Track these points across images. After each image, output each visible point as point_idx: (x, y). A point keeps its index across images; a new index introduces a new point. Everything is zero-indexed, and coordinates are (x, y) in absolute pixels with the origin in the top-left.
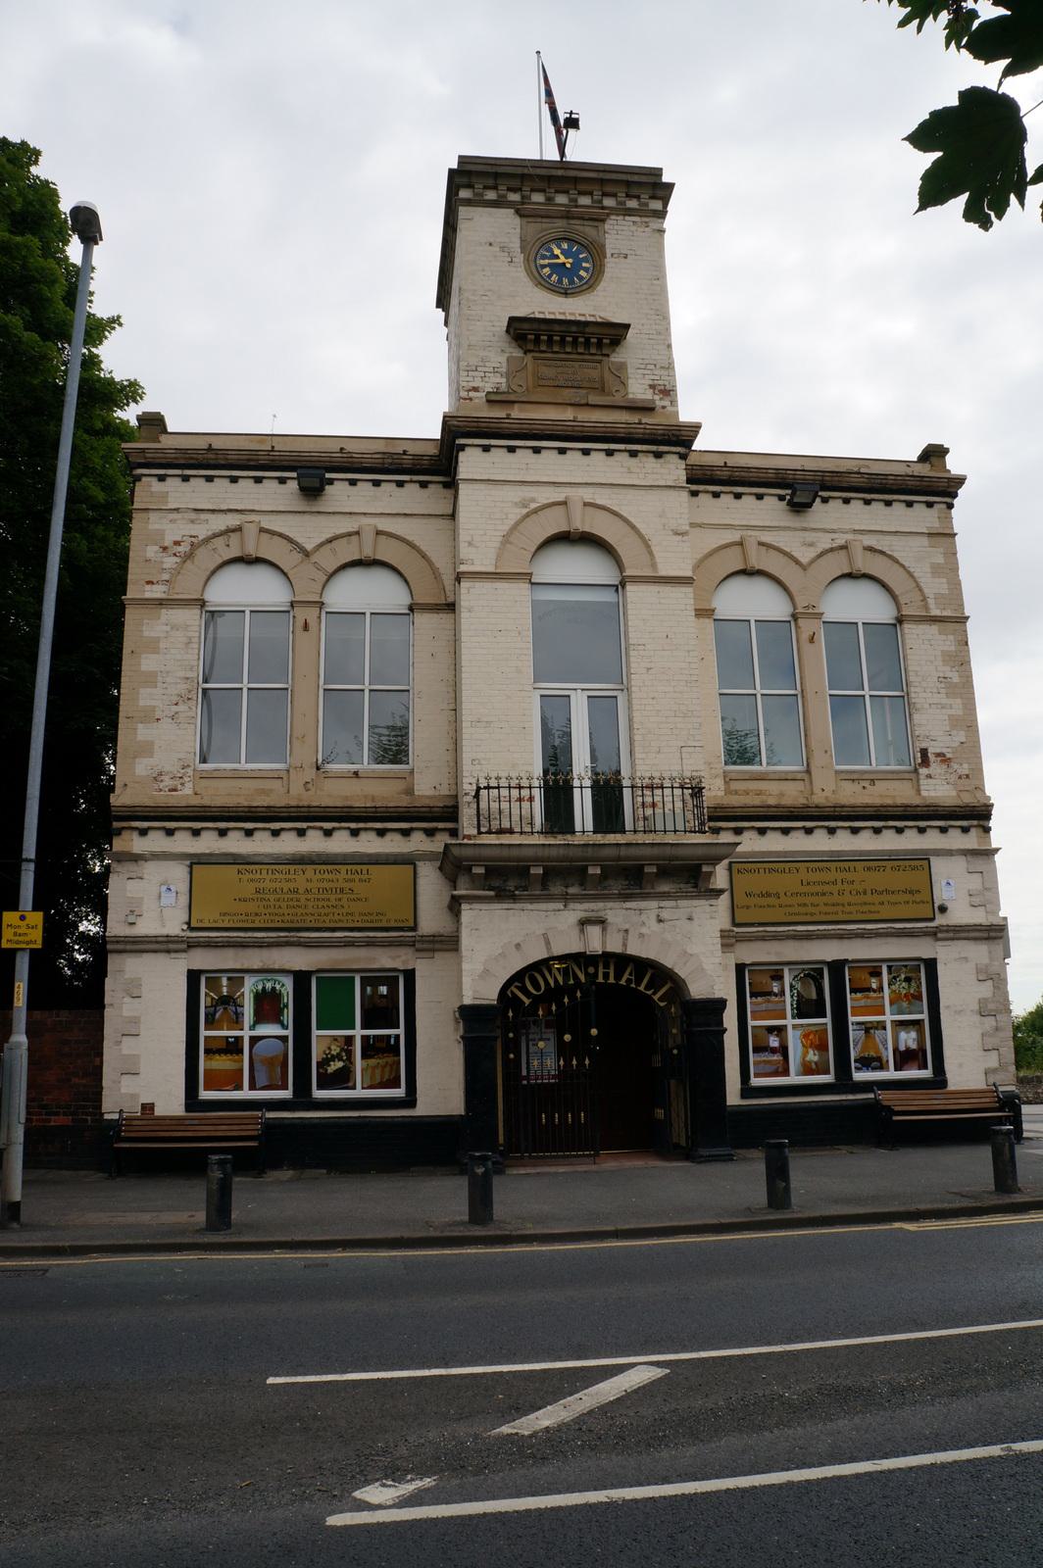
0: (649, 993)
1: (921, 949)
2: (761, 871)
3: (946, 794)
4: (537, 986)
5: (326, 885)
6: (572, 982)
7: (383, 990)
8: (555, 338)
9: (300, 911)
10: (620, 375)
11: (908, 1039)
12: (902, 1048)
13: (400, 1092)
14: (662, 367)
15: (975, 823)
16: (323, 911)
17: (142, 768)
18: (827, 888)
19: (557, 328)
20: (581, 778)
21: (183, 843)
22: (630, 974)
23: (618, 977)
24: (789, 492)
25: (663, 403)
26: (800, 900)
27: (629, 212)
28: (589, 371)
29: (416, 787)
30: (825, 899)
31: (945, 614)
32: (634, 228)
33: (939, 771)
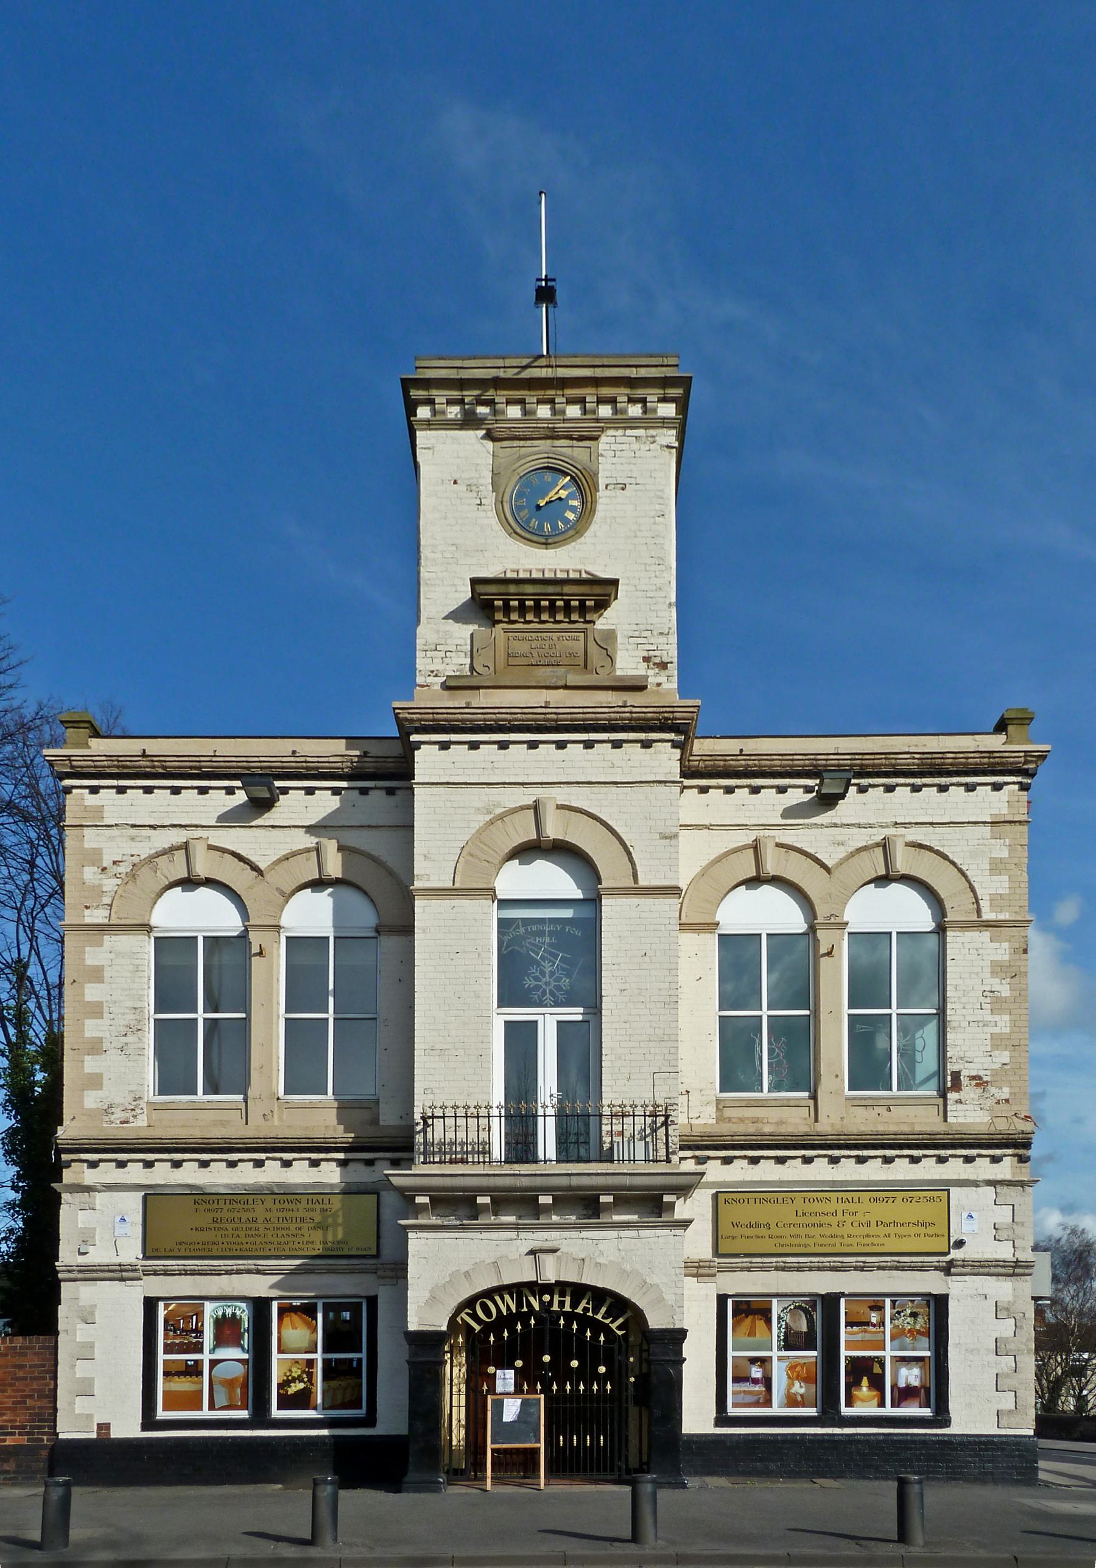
0: (607, 1321)
1: (932, 1283)
2: (752, 1201)
3: (978, 1120)
4: (488, 1313)
5: (284, 1214)
6: (525, 1309)
7: (347, 1315)
8: (527, 603)
9: (258, 1240)
10: (607, 643)
11: (911, 1376)
12: (902, 1384)
13: (361, 1412)
14: (661, 633)
15: (1010, 1151)
16: (283, 1240)
17: (92, 1100)
18: (825, 1219)
19: (529, 589)
20: (544, 1106)
21: (135, 1173)
22: (588, 1303)
23: (574, 1305)
24: (818, 781)
25: (659, 680)
26: (794, 1231)
27: (631, 423)
28: (570, 643)
29: (381, 1117)
30: (821, 1230)
31: (1001, 917)
32: (635, 446)
33: (972, 1095)
